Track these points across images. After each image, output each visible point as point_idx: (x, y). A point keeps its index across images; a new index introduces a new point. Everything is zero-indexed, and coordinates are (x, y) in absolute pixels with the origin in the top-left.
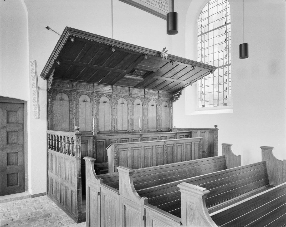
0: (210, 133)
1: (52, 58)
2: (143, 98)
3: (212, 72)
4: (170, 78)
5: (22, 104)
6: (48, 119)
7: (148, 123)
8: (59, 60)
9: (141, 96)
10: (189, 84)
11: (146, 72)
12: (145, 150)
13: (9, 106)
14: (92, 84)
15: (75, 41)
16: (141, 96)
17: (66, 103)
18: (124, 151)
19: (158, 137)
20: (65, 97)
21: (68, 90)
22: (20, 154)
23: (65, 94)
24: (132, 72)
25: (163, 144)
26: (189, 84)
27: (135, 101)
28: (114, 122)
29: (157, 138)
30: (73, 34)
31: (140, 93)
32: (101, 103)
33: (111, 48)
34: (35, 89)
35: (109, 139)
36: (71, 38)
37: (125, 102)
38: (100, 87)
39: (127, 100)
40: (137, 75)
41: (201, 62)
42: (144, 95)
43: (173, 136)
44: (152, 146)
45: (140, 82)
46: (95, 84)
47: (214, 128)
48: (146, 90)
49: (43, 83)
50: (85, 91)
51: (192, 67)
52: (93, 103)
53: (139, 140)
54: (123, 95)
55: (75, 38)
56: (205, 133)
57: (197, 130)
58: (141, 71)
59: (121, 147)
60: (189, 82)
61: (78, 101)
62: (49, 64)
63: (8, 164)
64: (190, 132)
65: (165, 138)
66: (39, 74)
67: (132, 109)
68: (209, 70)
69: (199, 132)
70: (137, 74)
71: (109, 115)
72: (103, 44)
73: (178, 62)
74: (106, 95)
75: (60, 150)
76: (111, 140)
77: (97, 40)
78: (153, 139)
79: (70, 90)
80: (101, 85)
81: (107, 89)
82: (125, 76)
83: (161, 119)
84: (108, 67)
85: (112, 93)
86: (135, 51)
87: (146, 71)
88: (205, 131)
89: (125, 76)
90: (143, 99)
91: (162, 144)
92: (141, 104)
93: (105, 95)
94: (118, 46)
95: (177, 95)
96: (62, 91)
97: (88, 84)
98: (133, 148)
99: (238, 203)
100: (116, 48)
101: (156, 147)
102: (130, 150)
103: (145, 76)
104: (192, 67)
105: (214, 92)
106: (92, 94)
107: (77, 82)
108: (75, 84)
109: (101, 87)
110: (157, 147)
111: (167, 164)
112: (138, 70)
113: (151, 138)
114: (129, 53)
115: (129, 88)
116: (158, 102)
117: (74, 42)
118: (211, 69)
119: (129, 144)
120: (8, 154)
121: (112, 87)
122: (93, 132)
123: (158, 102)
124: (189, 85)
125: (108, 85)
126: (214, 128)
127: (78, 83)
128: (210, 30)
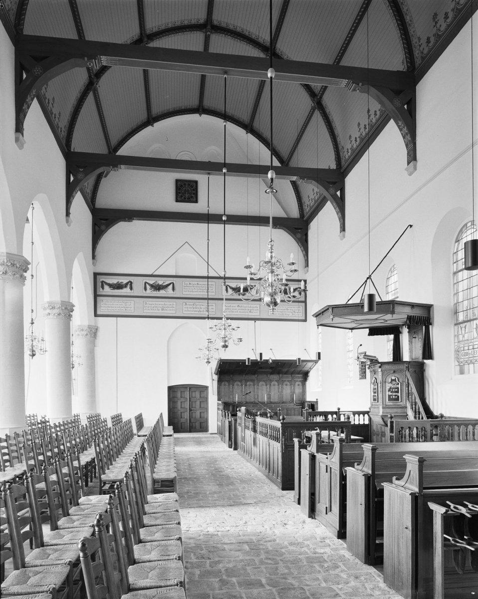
5: (206, 388)
6: (218, 395)
13: (201, 389)
17: (288, 387)
22: (205, 413)
34: (211, 381)
37: (265, 384)
47: (337, 411)
49: (216, 377)
61: (295, 385)
63: (200, 417)
66: (213, 373)
99: (308, 502)
108: (231, 376)
111: (190, 431)
120: (200, 413)
126: (337, 411)
128: (462, 272)
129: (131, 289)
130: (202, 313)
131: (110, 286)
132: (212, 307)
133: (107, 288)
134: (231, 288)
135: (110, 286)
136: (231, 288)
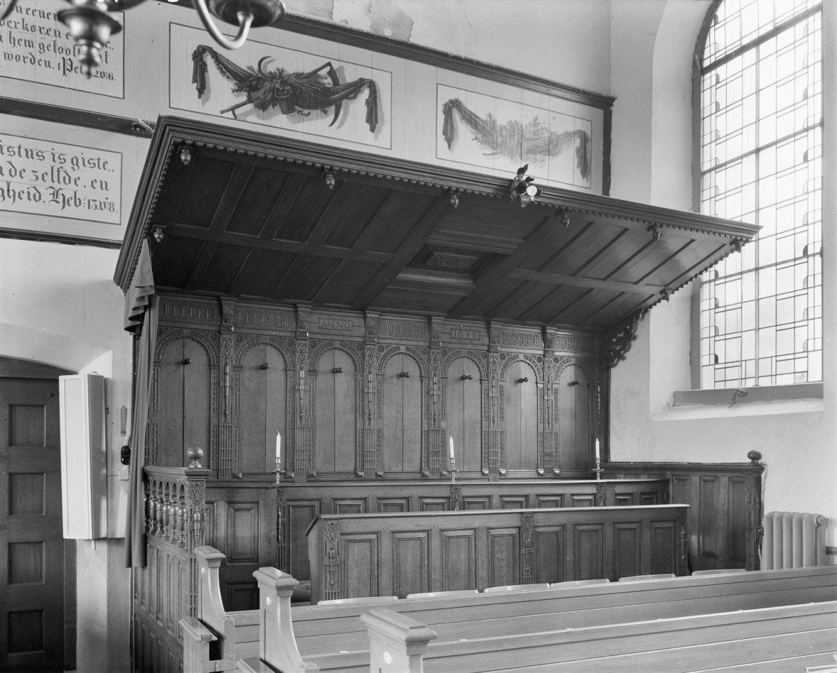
0: (733, 482)
1: (138, 219)
2: (539, 360)
3: (737, 245)
4: (604, 279)
7: (502, 445)
8: (160, 226)
9: (475, 347)
10: (659, 296)
11: (476, 258)
12: (446, 541)
14: (290, 309)
15: (339, 184)
16: (475, 347)
18: (363, 541)
19: (365, 499)
20: (275, 360)
21: (281, 336)
23: (195, 343)
24: (423, 260)
25: (519, 524)
26: (659, 296)
27: (453, 364)
28: (371, 441)
29: (522, 499)
30: (184, 136)
31: (471, 337)
32: (324, 373)
33: (321, 176)
35: (335, 499)
36: (180, 152)
38: (320, 316)
39: (419, 361)
40: (444, 269)
41: (714, 216)
42: (487, 342)
43: (485, 496)
44: (602, 524)
45: (462, 294)
46: (368, 315)
48: (493, 325)
50: (265, 332)
51: (648, 229)
52: (292, 373)
53: (657, 500)
54: (405, 342)
55: (194, 148)
56: (714, 481)
57: (687, 473)
58: (456, 253)
59: (351, 526)
60: (656, 290)
62: (131, 241)
64: (665, 483)
65: (443, 504)
67: (440, 393)
68: (727, 240)
69: (695, 479)
70: (445, 265)
71: (352, 416)
72: (203, 147)
73: (613, 217)
74: (407, 349)
75: (159, 528)
76: (340, 502)
77: (218, 142)
78: (543, 501)
79: (214, 328)
80: (323, 310)
81: (350, 324)
82: (402, 276)
83: (554, 431)
84: (331, 244)
85: (364, 337)
86: (410, 180)
87: (475, 253)
88: (714, 474)
89: (398, 276)
90: (539, 361)
91: (514, 525)
92: (476, 375)
93: (186, 332)
94: (346, 166)
95: (617, 343)
96: (186, 332)
97: (277, 308)
98: (444, 531)
100: (339, 174)
101: (441, 537)
102: (386, 543)
103: (474, 272)
104: (648, 229)
105: (757, 329)
106: (292, 344)
107: (311, 309)
109: (323, 316)
110: (398, 535)
112: (447, 249)
113: (495, 501)
114: (392, 190)
115: (429, 318)
116: (543, 368)
117: (190, 163)
118: (650, 219)
119: (381, 519)
121: (365, 318)
122: (275, 474)
123: (543, 368)
124: (659, 301)
125: (348, 309)
127: (240, 304)
129: (373, 118)
130: (71, 211)
131: (248, 82)
132: (99, 174)
133: (222, 91)
134: (227, 69)
135: (248, 82)
136: (227, 69)
